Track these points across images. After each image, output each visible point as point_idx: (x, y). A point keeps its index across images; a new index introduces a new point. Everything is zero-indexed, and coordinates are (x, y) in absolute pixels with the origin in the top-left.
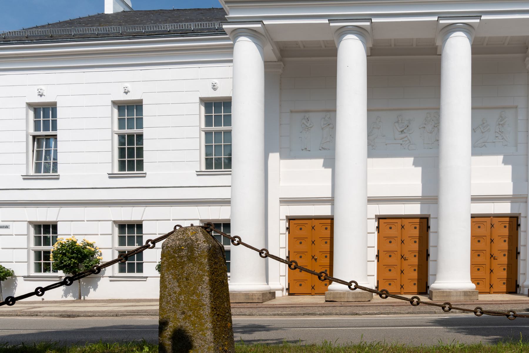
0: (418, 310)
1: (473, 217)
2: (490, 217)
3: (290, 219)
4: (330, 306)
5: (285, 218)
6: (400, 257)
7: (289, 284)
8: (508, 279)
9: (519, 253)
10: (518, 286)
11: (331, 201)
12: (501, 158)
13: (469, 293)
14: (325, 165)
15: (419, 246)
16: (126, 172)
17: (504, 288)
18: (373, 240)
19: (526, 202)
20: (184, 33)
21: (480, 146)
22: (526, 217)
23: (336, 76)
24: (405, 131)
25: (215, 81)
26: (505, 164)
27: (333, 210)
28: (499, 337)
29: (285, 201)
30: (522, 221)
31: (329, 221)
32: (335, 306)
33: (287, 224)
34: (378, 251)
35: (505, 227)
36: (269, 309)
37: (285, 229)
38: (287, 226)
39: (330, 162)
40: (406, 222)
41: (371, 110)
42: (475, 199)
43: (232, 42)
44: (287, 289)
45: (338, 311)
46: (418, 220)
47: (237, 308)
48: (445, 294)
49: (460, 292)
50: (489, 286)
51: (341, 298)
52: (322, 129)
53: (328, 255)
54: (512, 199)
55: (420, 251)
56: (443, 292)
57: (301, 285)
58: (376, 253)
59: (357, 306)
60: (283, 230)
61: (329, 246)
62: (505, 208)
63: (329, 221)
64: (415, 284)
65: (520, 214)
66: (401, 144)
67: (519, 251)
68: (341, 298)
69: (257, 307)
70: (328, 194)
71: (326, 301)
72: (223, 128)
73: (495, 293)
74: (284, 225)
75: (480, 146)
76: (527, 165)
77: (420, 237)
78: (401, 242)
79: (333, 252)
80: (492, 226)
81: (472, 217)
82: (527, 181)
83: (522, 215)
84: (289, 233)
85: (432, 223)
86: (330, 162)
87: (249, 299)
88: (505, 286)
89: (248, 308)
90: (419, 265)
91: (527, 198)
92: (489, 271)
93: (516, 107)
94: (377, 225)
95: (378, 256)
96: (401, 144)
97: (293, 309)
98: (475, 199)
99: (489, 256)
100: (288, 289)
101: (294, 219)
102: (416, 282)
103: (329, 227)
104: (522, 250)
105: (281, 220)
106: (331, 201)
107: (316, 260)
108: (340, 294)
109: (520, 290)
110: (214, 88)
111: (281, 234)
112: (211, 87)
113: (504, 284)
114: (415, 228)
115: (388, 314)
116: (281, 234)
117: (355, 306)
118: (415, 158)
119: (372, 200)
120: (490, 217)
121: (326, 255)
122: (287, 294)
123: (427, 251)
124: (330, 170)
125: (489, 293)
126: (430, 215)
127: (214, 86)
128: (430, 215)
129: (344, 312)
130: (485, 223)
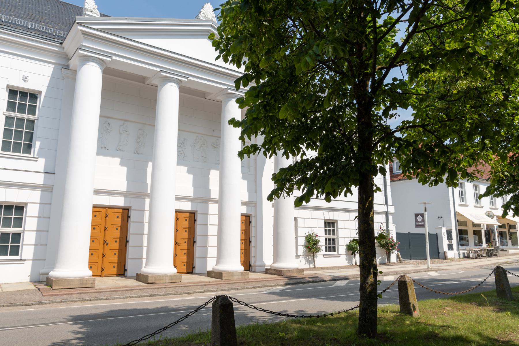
1: (95, 207)
12: (118, 160)
16: (11, 153)
17: (115, 271)
19: (52, 192)
20: (27, 30)
21: (103, 149)
26: (273, 179)
35: (186, 220)
42: (97, 192)
46: (121, 211)
49: (237, 273)
50: (100, 270)
52: (120, 134)
56: (229, 273)
62: (119, 202)
64: (114, 267)
65: (251, 214)
72: (26, 116)
75: (103, 149)
81: (94, 207)
82: (256, 192)
83: (253, 215)
85: (253, 220)
87: (83, 284)
91: (256, 204)
98: (97, 192)
99: (102, 242)
104: (253, 240)
107: (107, 244)
108: (160, 276)
110: (25, 80)
114: (186, 220)
120: (105, 208)
130: (100, 213)
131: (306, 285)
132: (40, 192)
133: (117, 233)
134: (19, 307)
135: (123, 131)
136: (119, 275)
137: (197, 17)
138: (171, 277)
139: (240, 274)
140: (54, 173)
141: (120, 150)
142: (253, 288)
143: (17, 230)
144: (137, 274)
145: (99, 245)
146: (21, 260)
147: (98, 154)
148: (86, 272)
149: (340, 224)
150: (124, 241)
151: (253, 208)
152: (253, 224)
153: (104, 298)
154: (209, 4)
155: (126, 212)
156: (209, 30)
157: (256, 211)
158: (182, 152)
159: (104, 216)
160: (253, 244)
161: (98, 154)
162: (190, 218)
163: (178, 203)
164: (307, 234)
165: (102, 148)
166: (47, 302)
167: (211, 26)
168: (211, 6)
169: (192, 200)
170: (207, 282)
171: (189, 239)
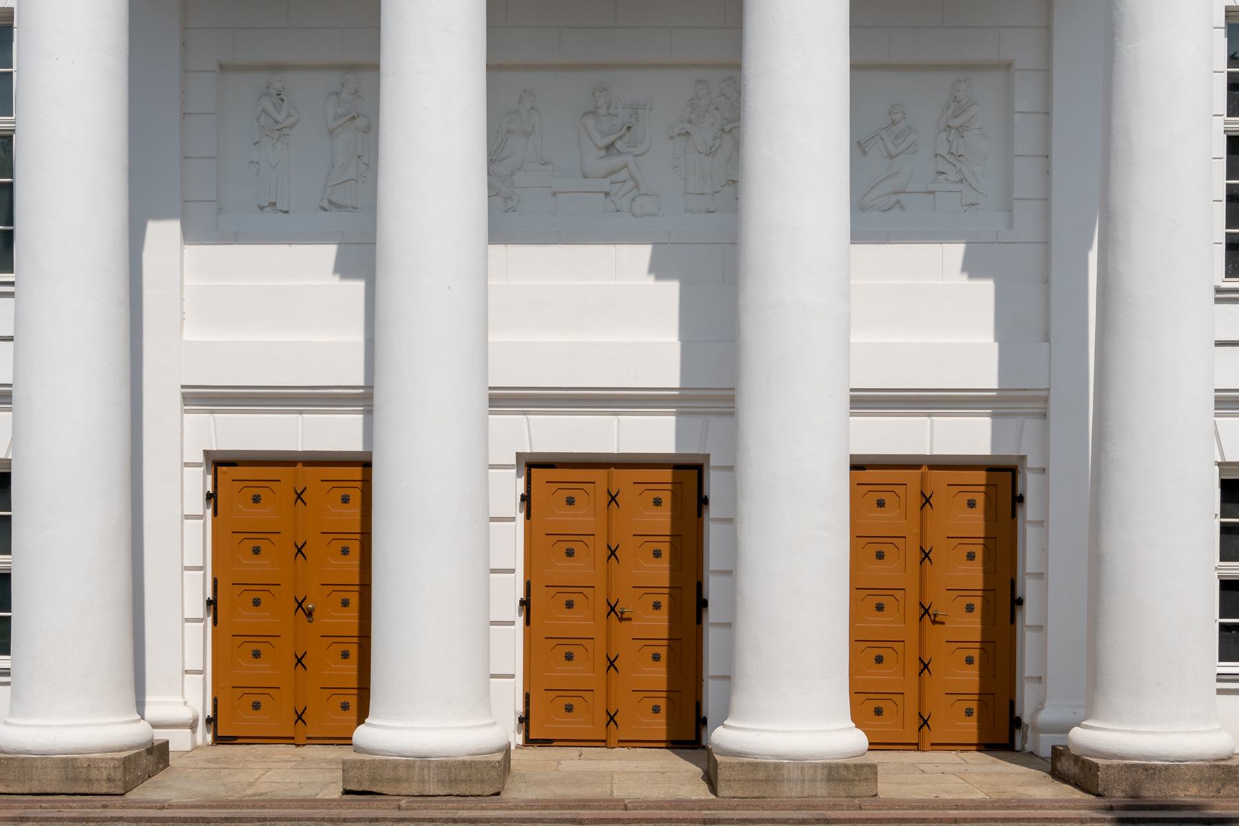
1: (858, 465)
2: (918, 467)
3: (218, 463)
5: (200, 458)
6: (606, 609)
7: (215, 700)
9: (1020, 602)
10: (1016, 723)
11: (362, 400)
12: (955, 252)
14: (344, 269)
19: (1044, 416)
24: (618, 145)
27: (369, 432)
29: (201, 398)
30: (1030, 485)
31: (357, 472)
32: (377, 820)
33: (210, 478)
37: (201, 498)
38: (210, 488)
39: (360, 258)
42: (866, 402)
46: (667, 475)
48: (761, 775)
49: (815, 766)
50: (916, 722)
53: (354, 650)
55: (675, 589)
56: (755, 766)
58: (521, 594)
60: (195, 502)
62: (972, 437)
63: (359, 468)
65: (1023, 458)
66: (607, 194)
68: (398, 780)
71: (346, 792)
74: (198, 482)
76: (1047, 281)
78: (606, 553)
82: (1047, 339)
83: (1030, 463)
84: (215, 513)
86: (360, 258)
87: (76, 780)
91: (1046, 400)
92: (917, 667)
93: (1008, 66)
95: (525, 604)
96: (607, 194)
98: (866, 402)
99: (916, 611)
100: (211, 721)
104: (1029, 589)
106: (362, 400)
107: (309, 614)
108: (396, 765)
109: (1024, 739)
119: (503, 400)
120: (918, 467)
122: (209, 738)
123: (700, 586)
124: (359, 286)
125: (917, 747)
126: (708, 456)
132: (987, 421)
133: (974, 575)
135: (337, 117)
136: (986, 746)
138: (840, 773)
139: (821, 775)
140: (1219, 344)
141: (339, 207)
144: (1054, 748)
145: (897, 623)
147: (858, 236)
148: (841, 738)
150: (1003, 602)
151: (1032, 425)
152: (1030, 510)
155: (1002, 483)
157: (733, 441)
158: (623, 175)
159: (916, 501)
160: (1029, 614)
161: (858, 236)
162: (991, 488)
165: (262, 208)
171: (988, 592)
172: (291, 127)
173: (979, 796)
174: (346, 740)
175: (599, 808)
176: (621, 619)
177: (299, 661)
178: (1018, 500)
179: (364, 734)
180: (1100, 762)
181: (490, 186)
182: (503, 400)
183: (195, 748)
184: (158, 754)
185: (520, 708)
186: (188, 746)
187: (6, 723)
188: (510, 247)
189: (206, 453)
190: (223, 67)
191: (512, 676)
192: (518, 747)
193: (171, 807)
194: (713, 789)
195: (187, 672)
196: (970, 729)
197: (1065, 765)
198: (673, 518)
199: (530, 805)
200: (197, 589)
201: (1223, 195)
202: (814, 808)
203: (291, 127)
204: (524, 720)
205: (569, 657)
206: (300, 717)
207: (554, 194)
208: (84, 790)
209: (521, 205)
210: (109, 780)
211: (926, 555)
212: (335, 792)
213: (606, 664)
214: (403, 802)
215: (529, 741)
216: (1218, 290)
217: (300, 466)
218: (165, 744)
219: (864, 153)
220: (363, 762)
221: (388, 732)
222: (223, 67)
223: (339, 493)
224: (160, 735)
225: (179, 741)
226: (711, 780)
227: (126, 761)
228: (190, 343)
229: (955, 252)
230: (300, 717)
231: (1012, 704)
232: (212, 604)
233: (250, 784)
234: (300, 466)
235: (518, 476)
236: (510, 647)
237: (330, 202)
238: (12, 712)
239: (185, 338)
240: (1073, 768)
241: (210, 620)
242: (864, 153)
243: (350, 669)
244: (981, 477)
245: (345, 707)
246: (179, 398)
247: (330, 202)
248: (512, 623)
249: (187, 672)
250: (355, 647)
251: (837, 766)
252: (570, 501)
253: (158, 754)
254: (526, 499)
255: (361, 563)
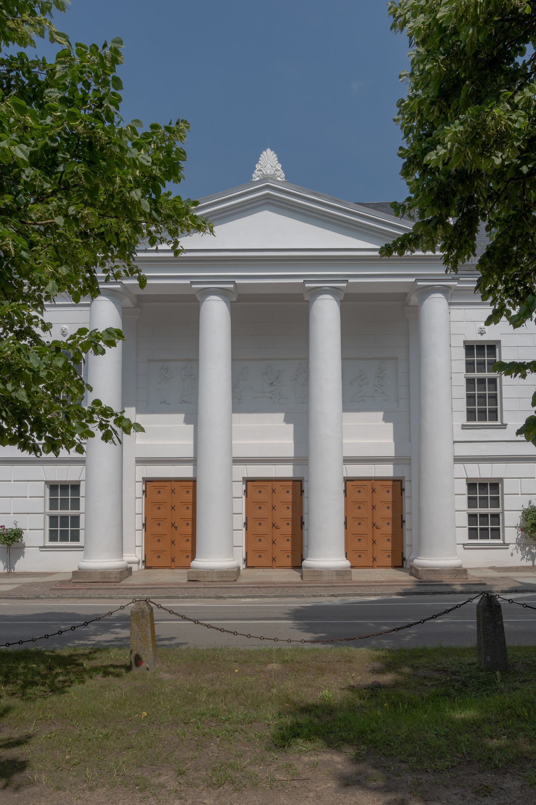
0: (286, 594)
2: (371, 480)
3: (147, 481)
4: (193, 588)
5: (141, 480)
6: (271, 525)
7: (145, 555)
8: (393, 551)
9: (404, 522)
10: (404, 559)
11: (194, 461)
12: (381, 414)
13: (341, 573)
14: (187, 421)
15: (292, 512)
18: (240, 505)
19: (410, 464)
21: (352, 402)
22: (410, 481)
23: (198, 323)
24: (274, 383)
25: (65, 326)
27: (195, 471)
28: (324, 635)
29: (140, 461)
30: (406, 485)
31: (191, 484)
32: (198, 588)
33: (144, 486)
34: (246, 518)
35: (388, 491)
36: (128, 591)
37: (141, 492)
38: (144, 489)
39: (193, 417)
40: (277, 484)
41: (235, 359)
42: (347, 460)
43: (89, 302)
44: (143, 562)
45: (201, 594)
46: (291, 483)
47: (94, 589)
48: (316, 574)
49: (332, 571)
50: (372, 559)
51: (205, 577)
53: (190, 523)
54: (395, 461)
55: (293, 519)
56: (314, 571)
57: (159, 557)
58: (244, 521)
59: (222, 588)
60: (139, 493)
61: (192, 495)
62: (387, 471)
63: (191, 484)
64: (288, 557)
66: (271, 398)
67: (404, 519)
68: (205, 577)
69: (115, 589)
70: (189, 453)
71: (189, 581)
73: (379, 567)
74: (140, 487)
75: (352, 402)
76: (410, 423)
77: (294, 503)
78: (271, 508)
79: (195, 535)
80: (374, 490)
82: (410, 441)
83: (406, 479)
84: (146, 497)
86: (193, 417)
88: (390, 560)
89: (106, 589)
90: (293, 535)
91: (410, 459)
92: (371, 542)
93: (397, 358)
94: (244, 488)
95: (246, 524)
96: (271, 398)
97: (153, 590)
98: (347, 460)
99: (371, 525)
100: (144, 562)
101: (152, 481)
102: (290, 554)
103: (191, 491)
104: (407, 518)
105: (137, 482)
106: (194, 461)
107: (176, 528)
108: (204, 572)
109: (406, 564)
111: (137, 498)
112: (60, 333)
113: (389, 556)
115: (254, 597)
116: (137, 498)
117: (219, 588)
118: (286, 413)
119: (237, 461)
120: (371, 480)
121: (187, 538)
122: (143, 567)
123: (302, 518)
124: (191, 427)
125: (372, 567)
126: (304, 478)
127: (64, 332)
128: (304, 478)
129: (208, 595)
130: (365, 487)
131: (438, 597)
134: (20, 601)
136: (395, 567)
137: (249, 181)
138: (340, 573)
142: (333, 595)
143: (495, 510)
146: (504, 544)
148: (343, 563)
149: (508, 487)
150: (399, 522)
152: (406, 493)
153: (106, 596)
154: (268, 150)
155: (397, 485)
156: (268, 194)
163: (459, 467)
164: (527, 506)
166: (44, 596)
167: (268, 187)
168: (272, 153)
169: (395, 461)
170: (403, 581)
171: (394, 519)
172: (170, 378)
173: (383, 579)
174: (189, 567)
175: (266, 584)
176: (277, 528)
177: (173, 542)
178: (403, 490)
179: (194, 564)
180: (419, 569)
181: (233, 396)
182: (237, 461)
183: (139, 570)
184: (129, 571)
185: (244, 556)
186: (137, 570)
187: (83, 561)
188: (240, 414)
189: (143, 478)
190: (149, 360)
191: (242, 547)
192: (243, 569)
193: (135, 585)
194: (302, 579)
195: (136, 546)
196: (389, 561)
197: (413, 571)
198: (293, 497)
199: (245, 584)
200: (139, 521)
201: (465, 396)
202: (331, 583)
203: (170, 378)
204: (246, 560)
205: (260, 540)
206: (173, 560)
207: (254, 398)
208: (108, 581)
209: (243, 400)
210: (115, 578)
211: (374, 507)
212: (185, 581)
213: (272, 542)
214: (206, 583)
215: (247, 567)
216: (463, 425)
217: (173, 482)
218: (131, 568)
219: (352, 385)
220: (194, 571)
221: (201, 563)
222: (149, 360)
223: (186, 490)
224: (129, 565)
225: (135, 568)
226: (302, 577)
227: (121, 572)
228: (138, 444)
229: (381, 414)
230: (173, 560)
231: (402, 553)
232: (144, 525)
233: (158, 579)
234: (173, 482)
235: (243, 484)
236: (240, 537)
237: (183, 401)
238: (84, 558)
239: (137, 443)
240: (414, 571)
241: (144, 530)
242: (352, 385)
243: (189, 545)
244: (391, 483)
245: (188, 557)
246: (134, 461)
247: (183, 401)
248: (242, 530)
249: (136, 546)
250: (192, 490)
251: (339, 571)
252: (260, 492)
253: (129, 571)
254: (246, 491)
255: (193, 513)
